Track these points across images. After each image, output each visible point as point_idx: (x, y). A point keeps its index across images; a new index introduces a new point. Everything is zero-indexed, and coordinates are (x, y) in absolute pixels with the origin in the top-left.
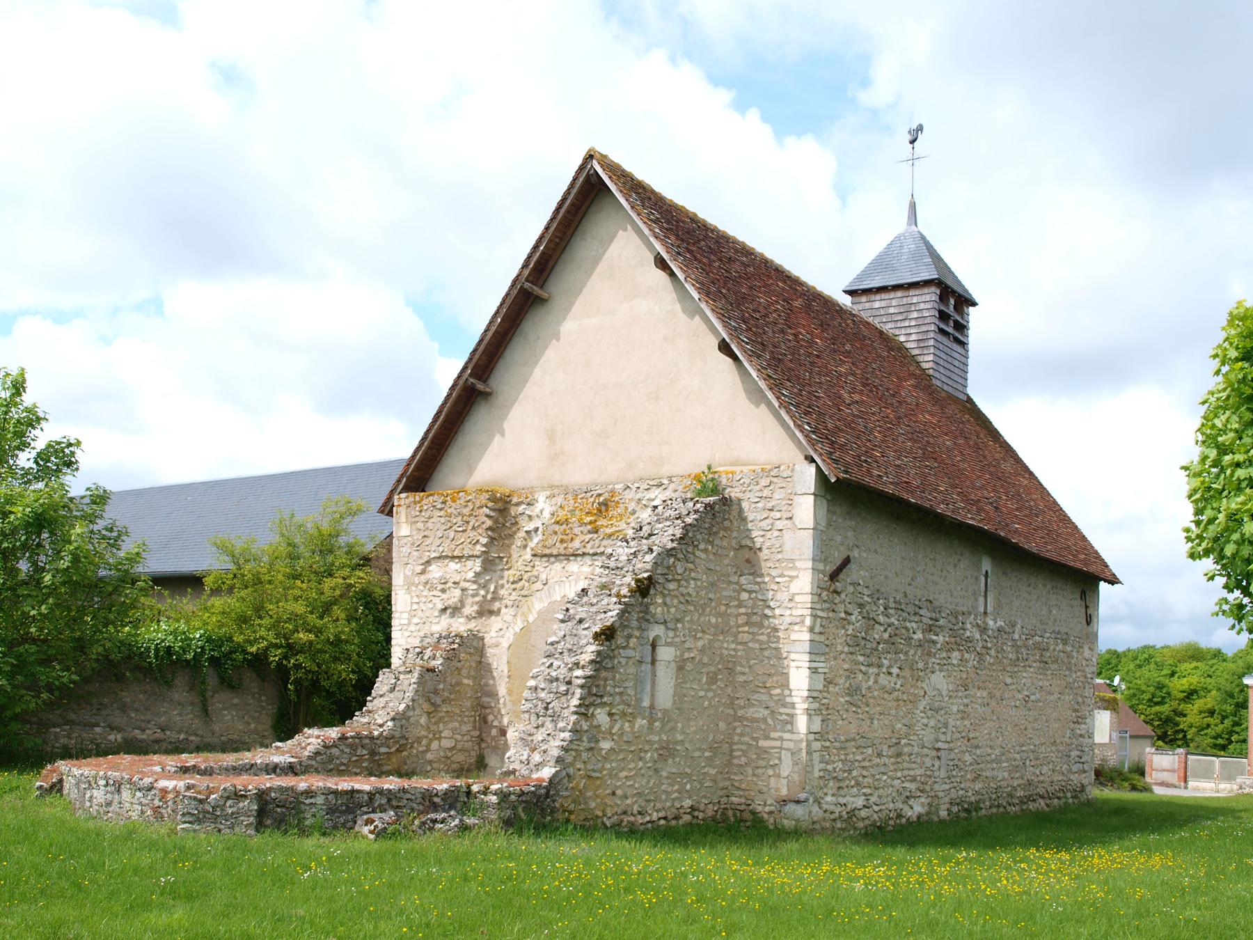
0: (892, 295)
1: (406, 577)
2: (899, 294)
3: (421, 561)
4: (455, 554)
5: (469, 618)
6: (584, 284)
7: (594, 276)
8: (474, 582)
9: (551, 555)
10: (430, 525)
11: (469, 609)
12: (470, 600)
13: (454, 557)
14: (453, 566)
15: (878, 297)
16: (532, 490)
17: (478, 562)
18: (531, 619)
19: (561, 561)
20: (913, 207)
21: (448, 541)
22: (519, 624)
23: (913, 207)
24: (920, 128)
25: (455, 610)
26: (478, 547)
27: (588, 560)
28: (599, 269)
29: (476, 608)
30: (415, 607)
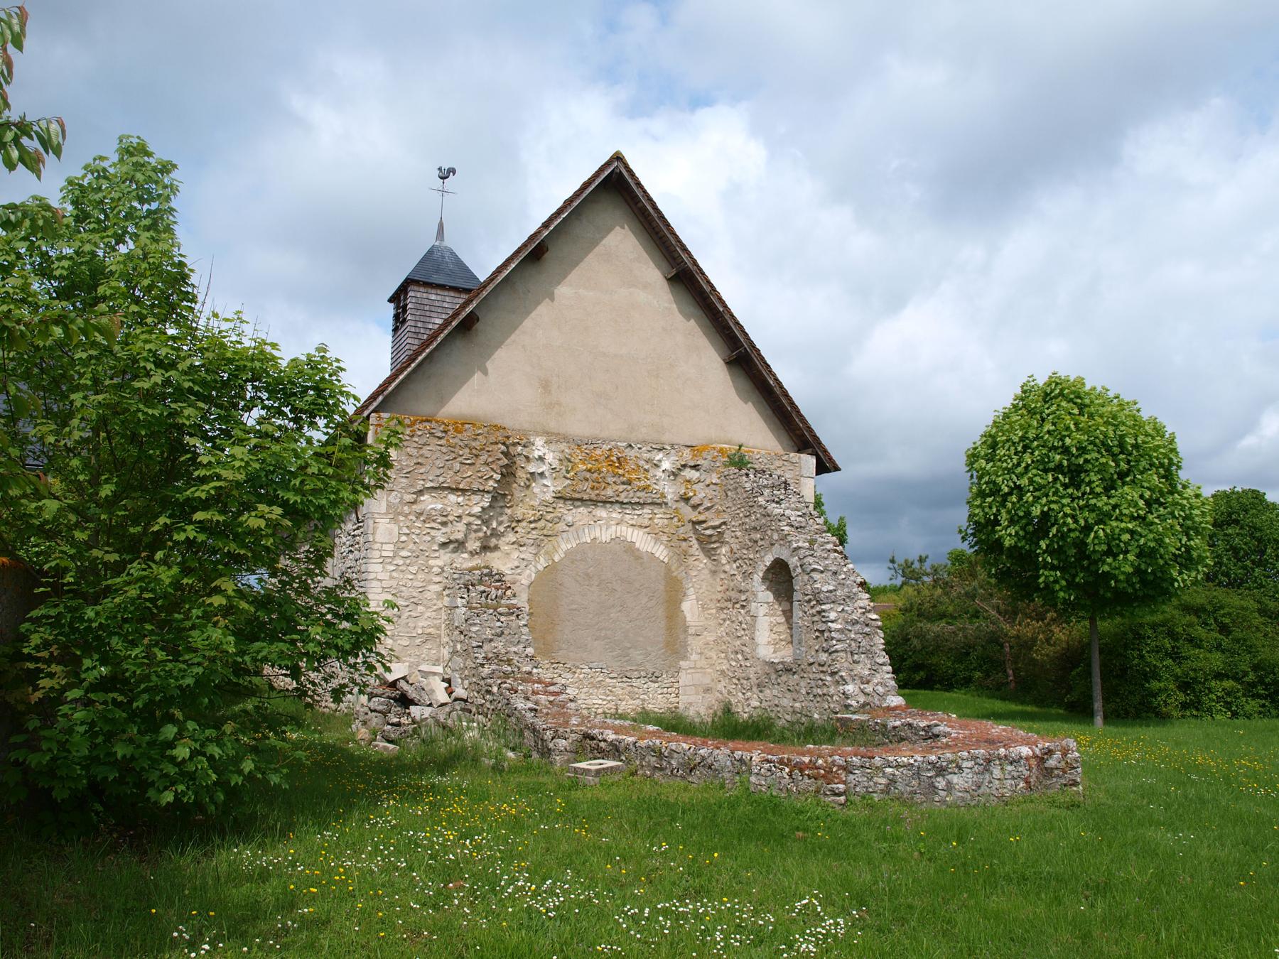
0: (446, 293)
1: (389, 506)
2: (452, 294)
3: (414, 490)
4: (461, 486)
5: (472, 554)
6: (581, 260)
7: (591, 256)
8: (479, 517)
9: (581, 500)
10: (424, 451)
11: (473, 545)
12: (473, 535)
13: (458, 489)
14: (453, 498)
15: (434, 291)
16: (526, 433)
17: (488, 498)
18: (557, 559)
19: (587, 506)
20: (441, 227)
21: (451, 473)
22: (542, 563)
23: (441, 227)
24: (452, 171)
25: (460, 545)
26: (491, 483)
27: (617, 507)
28: (596, 250)
29: (478, 544)
30: (404, 538)
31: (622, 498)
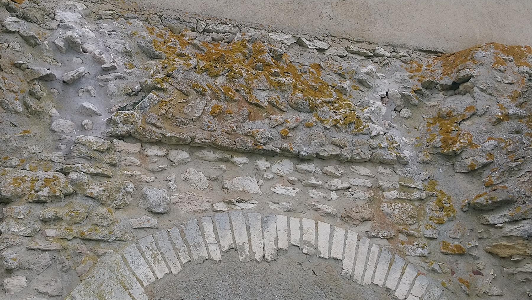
31: (299, 142)
